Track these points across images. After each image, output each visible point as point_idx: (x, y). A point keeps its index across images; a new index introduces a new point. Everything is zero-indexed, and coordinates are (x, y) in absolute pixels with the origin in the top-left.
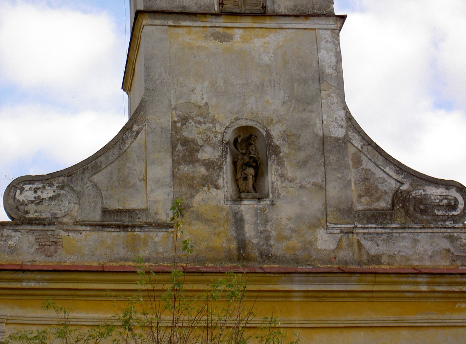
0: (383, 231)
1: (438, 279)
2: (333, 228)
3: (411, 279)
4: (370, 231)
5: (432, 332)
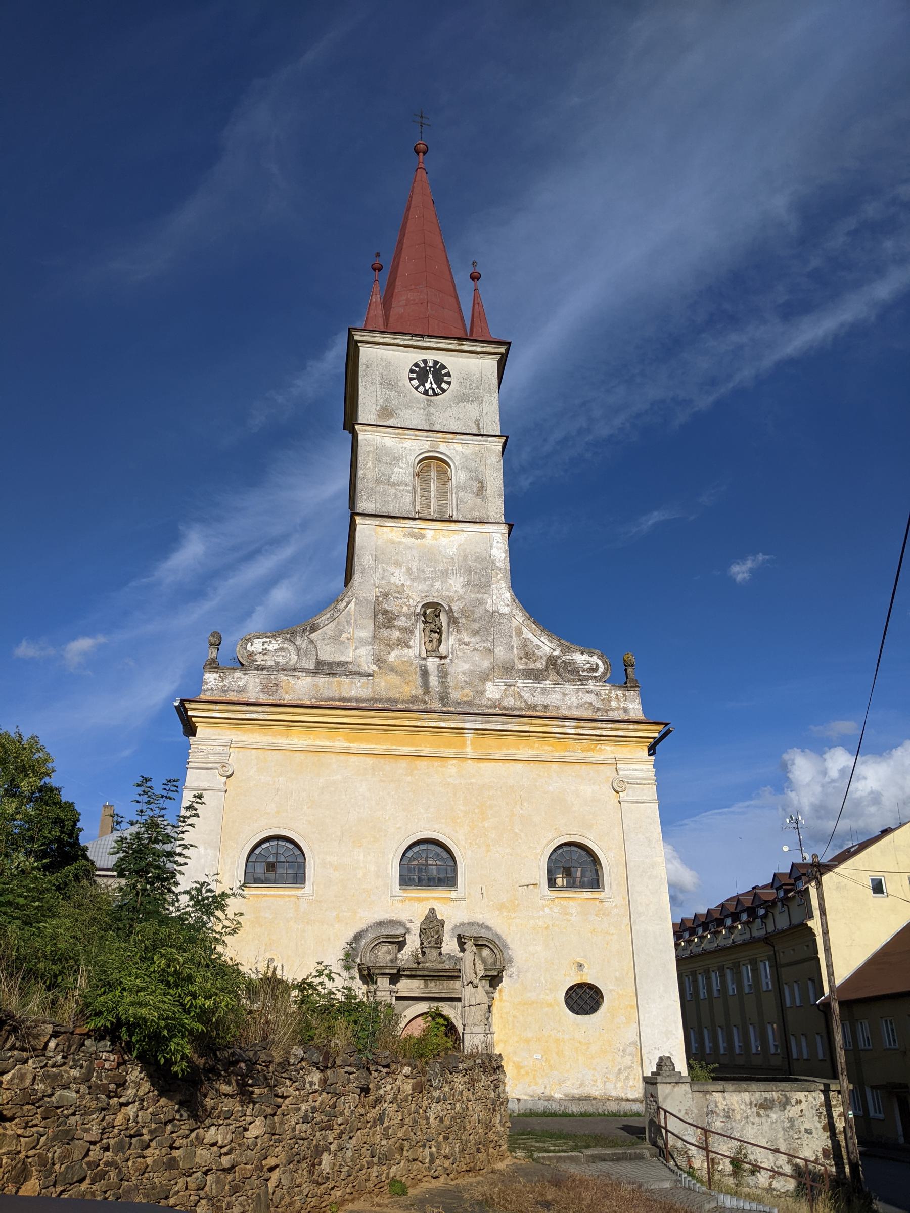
0: (539, 685)
1: (582, 724)
2: (499, 682)
3: (560, 723)
4: (528, 685)
5: (577, 766)
